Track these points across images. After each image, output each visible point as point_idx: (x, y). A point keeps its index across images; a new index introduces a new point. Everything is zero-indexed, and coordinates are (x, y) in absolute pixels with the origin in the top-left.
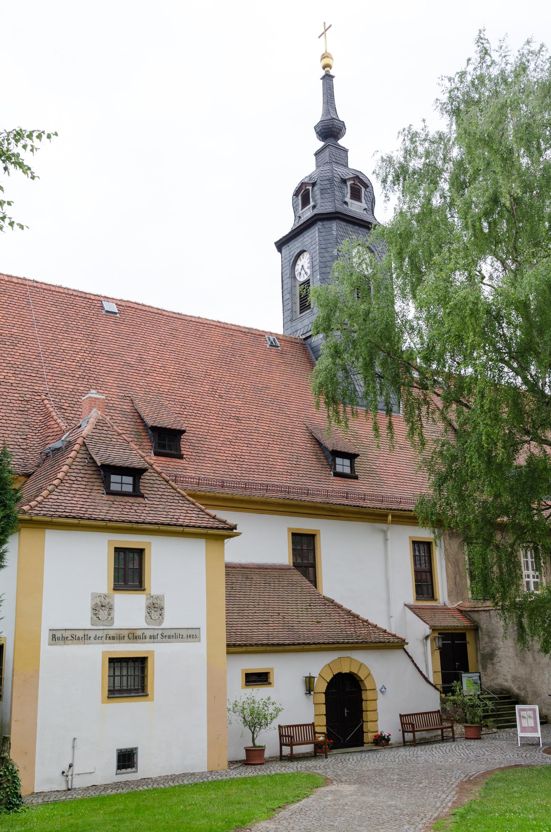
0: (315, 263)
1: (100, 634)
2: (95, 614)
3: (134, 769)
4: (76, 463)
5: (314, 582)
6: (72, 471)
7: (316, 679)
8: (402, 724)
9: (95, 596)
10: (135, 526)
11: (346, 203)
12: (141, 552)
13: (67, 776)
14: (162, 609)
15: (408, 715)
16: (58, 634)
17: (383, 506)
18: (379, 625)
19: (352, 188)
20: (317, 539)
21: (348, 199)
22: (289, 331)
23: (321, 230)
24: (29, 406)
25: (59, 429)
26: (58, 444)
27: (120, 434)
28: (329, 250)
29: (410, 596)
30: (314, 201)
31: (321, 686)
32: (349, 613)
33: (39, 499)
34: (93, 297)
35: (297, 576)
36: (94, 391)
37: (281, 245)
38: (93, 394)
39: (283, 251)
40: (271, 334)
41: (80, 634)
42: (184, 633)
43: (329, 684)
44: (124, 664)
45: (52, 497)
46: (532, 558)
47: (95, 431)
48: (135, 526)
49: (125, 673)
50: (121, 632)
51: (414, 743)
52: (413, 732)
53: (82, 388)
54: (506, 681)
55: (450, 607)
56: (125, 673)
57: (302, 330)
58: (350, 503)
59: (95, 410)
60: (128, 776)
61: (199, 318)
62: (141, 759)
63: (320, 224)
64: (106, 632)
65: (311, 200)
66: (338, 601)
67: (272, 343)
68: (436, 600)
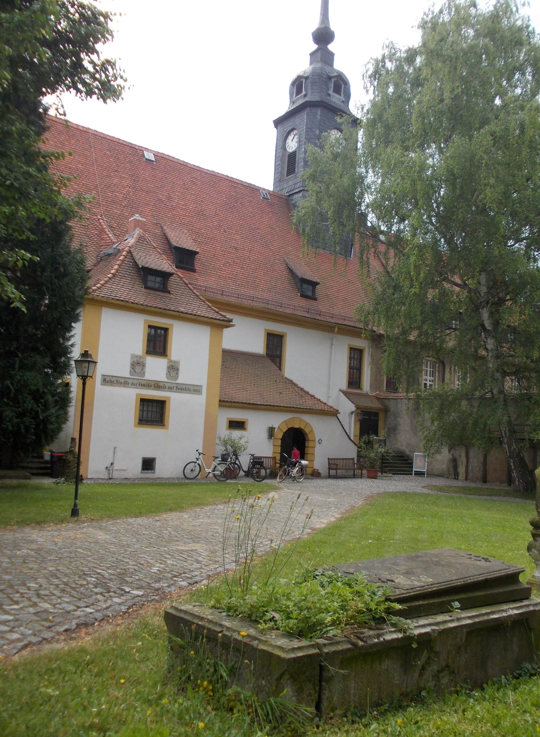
0: (302, 139)
1: (135, 382)
2: (133, 368)
3: (153, 471)
4: (124, 265)
5: (280, 368)
6: (121, 269)
7: (276, 429)
8: (329, 464)
9: (133, 356)
10: (164, 311)
11: (329, 95)
12: (166, 330)
13: (109, 470)
14: (178, 370)
15: (333, 459)
16: (108, 379)
17: (333, 321)
18: (322, 400)
19: (335, 83)
20: (284, 339)
21: (331, 92)
22: (278, 189)
23: (309, 114)
24: (89, 223)
25: (110, 241)
26: (110, 251)
27: (155, 248)
28: (313, 130)
29: (343, 384)
30: (306, 90)
31: (279, 435)
32: (302, 389)
33: (98, 285)
34: (137, 148)
35: (268, 362)
36: (138, 215)
37: (278, 123)
38: (137, 217)
39: (279, 127)
40: (264, 189)
41: (122, 381)
42: (192, 388)
43: (284, 433)
44: (150, 404)
45: (108, 285)
46: (430, 368)
47: (137, 243)
48: (164, 311)
49: (150, 409)
50: (151, 382)
51: (336, 477)
52: (336, 469)
53: (127, 214)
54: (402, 445)
55: (370, 395)
56: (150, 409)
57: (287, 189)
58: (310, 316)
59: (138, 229)
60: (148, 475)
61: (213, 171)
62: (158, 465)
63: (309, 109)
64: (139, 381)
65: (303, 90)
66: (294, 381)
67: (264, 195)
68: (362, 389)
